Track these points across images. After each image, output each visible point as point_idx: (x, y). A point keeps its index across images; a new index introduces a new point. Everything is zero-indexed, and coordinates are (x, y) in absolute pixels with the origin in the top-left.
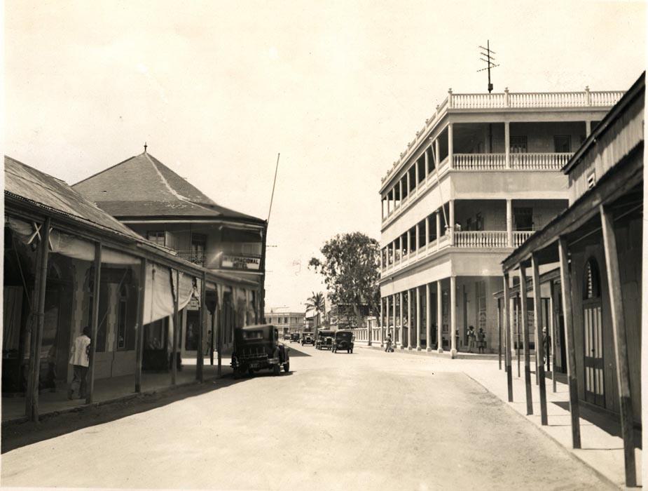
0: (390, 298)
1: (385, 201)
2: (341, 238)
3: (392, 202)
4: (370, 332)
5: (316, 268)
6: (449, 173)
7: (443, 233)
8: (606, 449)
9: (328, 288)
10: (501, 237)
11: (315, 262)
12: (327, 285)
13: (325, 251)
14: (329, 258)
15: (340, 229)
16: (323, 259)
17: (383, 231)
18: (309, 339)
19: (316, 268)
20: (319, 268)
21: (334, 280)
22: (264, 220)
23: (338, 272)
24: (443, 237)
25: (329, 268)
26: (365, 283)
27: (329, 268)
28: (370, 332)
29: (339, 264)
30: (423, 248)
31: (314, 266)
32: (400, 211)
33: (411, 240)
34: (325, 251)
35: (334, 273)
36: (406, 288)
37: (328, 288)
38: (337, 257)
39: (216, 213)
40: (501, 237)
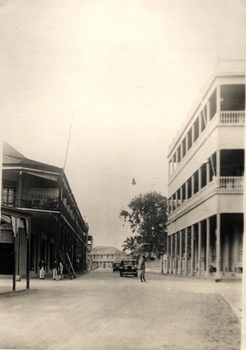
0: (173, 235)
1: (171, 163)
2: (143, 196)
3: (175, 164)
4: (163, 263)
5: (125, 218)
6: (218, 126)
7: (211, 180)
8: (181, 171)
9: (133, 231)
10: (233, 117)
11: (124, 214)
12: (132, 230)
13: (130, 206)
14: (134, 210)
15: (142, 190)
16: (130, 211)
17: (168, 186)
18: (129, 267)
19: (125, 218)
20: (128, 218)
21: (138, 227)
22: (61, 168)
23: (142, 220)
24: (211, 182)
25: (135, 218)
26: (160, 228)
27: (135, 218)
28: (163, 263)
29: (142, 214)
30: (197, 193)
31: (124, 217)
32: (180, 168)
33: (189, 190)
34: (130, 206)
35: (138, 221)
36: (185, 226)
37: (133, 231)
38: (141, 210)
39: (18, 161)
40: (233, 117)
